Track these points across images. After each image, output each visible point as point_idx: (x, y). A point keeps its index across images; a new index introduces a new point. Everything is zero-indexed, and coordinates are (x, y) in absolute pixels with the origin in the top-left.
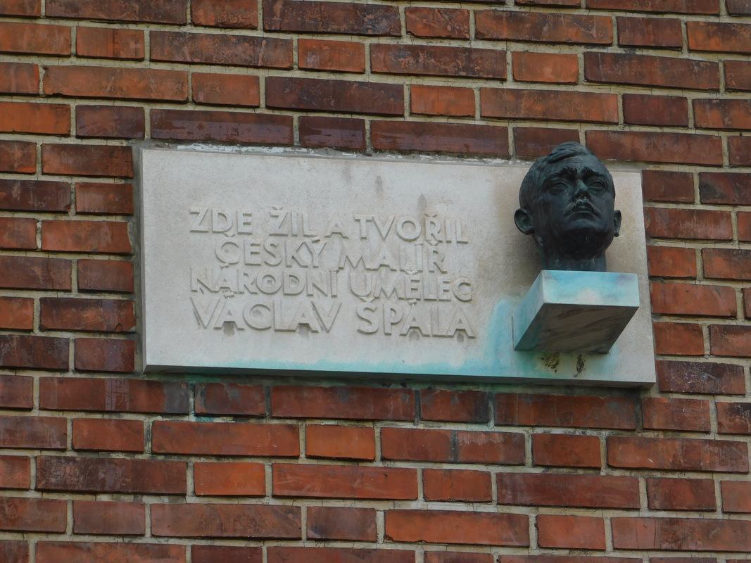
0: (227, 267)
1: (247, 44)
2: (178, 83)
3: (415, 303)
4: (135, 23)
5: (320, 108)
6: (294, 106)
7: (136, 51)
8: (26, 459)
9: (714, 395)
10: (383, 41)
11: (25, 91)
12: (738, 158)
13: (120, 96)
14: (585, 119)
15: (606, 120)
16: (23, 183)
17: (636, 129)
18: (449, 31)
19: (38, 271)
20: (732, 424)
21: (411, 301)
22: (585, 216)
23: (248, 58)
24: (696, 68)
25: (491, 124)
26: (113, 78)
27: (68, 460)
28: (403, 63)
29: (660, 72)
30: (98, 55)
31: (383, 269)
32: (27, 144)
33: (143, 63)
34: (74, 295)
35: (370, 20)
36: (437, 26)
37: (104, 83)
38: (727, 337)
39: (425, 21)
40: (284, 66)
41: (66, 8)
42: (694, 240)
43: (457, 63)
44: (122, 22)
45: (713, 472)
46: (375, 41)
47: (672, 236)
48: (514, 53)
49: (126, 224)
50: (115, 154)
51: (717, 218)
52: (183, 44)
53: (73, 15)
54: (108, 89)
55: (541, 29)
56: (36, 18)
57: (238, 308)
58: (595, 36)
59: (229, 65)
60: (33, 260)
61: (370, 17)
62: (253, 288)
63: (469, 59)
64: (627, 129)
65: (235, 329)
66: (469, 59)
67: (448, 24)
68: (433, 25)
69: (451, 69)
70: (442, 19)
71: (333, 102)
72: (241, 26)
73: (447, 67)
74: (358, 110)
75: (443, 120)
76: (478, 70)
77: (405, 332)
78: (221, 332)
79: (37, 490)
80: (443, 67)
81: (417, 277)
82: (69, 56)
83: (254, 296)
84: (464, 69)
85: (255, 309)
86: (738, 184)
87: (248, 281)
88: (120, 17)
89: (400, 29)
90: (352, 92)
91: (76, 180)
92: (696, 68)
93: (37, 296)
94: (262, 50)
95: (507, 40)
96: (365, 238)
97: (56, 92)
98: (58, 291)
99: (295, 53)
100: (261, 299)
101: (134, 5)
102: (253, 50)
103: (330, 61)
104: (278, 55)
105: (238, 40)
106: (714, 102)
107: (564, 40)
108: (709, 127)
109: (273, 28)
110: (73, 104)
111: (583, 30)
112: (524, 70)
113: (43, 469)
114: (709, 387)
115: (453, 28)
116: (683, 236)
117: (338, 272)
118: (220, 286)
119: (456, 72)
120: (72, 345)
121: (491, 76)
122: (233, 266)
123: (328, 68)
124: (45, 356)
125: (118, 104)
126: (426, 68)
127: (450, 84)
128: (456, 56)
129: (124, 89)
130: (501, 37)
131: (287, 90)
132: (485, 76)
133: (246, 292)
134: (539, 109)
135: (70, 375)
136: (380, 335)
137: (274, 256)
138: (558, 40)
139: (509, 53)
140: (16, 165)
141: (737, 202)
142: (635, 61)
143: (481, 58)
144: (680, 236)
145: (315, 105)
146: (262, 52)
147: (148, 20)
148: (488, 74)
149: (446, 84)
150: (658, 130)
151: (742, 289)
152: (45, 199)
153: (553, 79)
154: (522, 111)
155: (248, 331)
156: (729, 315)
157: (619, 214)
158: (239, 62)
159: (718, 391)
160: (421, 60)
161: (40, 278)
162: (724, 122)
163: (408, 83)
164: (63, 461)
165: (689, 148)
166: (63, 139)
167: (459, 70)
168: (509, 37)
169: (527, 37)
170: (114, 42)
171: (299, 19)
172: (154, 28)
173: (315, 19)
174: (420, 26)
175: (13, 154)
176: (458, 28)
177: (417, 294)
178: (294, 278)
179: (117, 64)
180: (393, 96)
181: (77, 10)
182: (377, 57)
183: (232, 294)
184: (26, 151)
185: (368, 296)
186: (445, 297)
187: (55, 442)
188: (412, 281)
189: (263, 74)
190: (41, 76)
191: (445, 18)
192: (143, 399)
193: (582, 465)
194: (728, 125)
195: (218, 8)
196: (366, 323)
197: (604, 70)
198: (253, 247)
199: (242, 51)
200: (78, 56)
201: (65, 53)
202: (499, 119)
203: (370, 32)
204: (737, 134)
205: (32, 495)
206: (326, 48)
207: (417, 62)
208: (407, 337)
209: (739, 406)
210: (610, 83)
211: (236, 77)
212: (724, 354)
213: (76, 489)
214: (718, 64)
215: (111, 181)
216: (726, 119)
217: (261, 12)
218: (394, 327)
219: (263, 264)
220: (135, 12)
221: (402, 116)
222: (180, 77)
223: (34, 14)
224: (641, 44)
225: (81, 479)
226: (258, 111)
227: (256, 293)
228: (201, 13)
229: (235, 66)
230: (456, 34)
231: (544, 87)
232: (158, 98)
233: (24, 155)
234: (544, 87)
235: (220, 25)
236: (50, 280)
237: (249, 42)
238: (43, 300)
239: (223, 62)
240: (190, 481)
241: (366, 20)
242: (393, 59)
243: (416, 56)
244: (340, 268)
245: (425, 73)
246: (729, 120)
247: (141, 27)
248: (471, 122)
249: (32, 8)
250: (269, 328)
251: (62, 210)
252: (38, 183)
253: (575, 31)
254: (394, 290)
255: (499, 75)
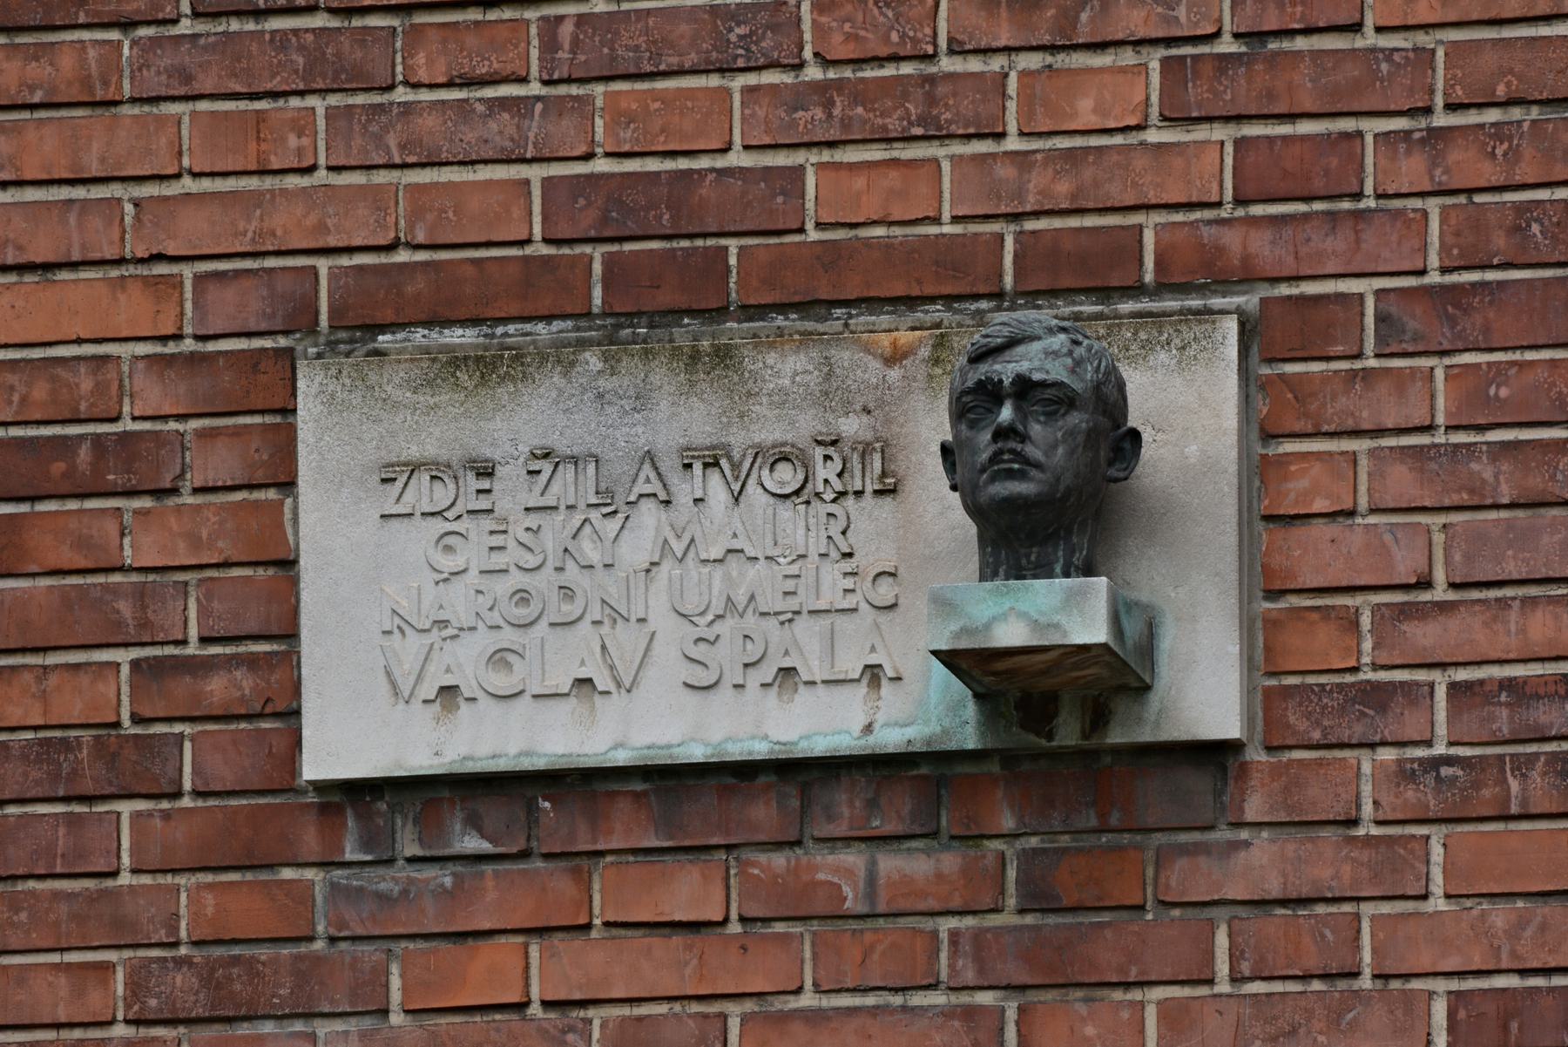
0: (446, 580)
1: (506, 116)
2: (379, 209)
3: (790, 621)
4: (301, 94)
5: (640, 233)
6: (593, 233)
7: (300, 151)
8: (108, 967)
9: (1372, 746)
10: (770, 78)
11: (97, 256)
12: (1455, 252)
13: (271, 248)
14: (1154, 201)
15: (1194, 199)
16: (97, 439)
17: (1258, 210)
18: (892, 44)
19: (125, 608)
20: (1399, 802)
21: (782, 618)
22: (1010, 475)
23: (508, 144)
24: (1384, 67)
25: (974, 228)
26: (258, 212)
27: (180, 962)
28: (802, 122)
29: (1309, 85)
30: (230, 168)
31: (733, 562)
32: (105, 358)
33: (316, 174)
34: (192, 649)
35: (741, 37)
36: (870, 36)
37: (241, 225)
38: (1404, 627)
39: (847, 26)
40: (576, 153)
41: (169, 77)
42: (1356, 433)
43: (907, 109)
44: (274, 95)
45: (1358, 899)
46: (752, 79)
47: (1310, 429)
48: (1024, 74)
49: (282, 503)
50: (262, 367)
51: (1401, 380)
52: (386, 129)
53: (182, 91)
54: (250, 234)
55: (1077, 17)
56: (115, 103)
57: (465, 661)
58: (1183, 19)
59: (473, 163)
60: (113, 590)
61: (740, 31)
62: (495, 618)
63: (931, 100)
64: (1240, 212)
65: (460, 700)
66: (931, 100)
67: (893, 28)
68: (862, 33)
69: (894, 125)
70: (882, 19)
71: (666, 217)
72: (497, 77)
73: (888, 120)
74: (713, 229)
75: (880, 231)
76: (946, 121)
77: (769, 680)
78: (437, 707)
79: (127, 1022)
80: (880, 121)
81: (794, 569)
82: (178, 176)
83: (494, 633)
84: (922, 121)
85: (498, 656)
86: (1450, 309)
87: (484, 602)
88: (269, 86)
89: (802, 49)
90: (704, 192)
91: (194, 424)
92: (1384, 67)
93: (123, 656)
94: (535, 124)
95: (1008, 50)
96: (701, 500)
97: (155, 252)
98: (162, 643)
99: (599, 122)
100: (509, 637)
101: (294, 57)
102: (518, 127)
103: (663, 131)
104: (566, 133)
105: (490, 108)
106: (1417, 135)
107: (1120, 36)
108: (1403, 191)
109: (556, 77)
110: (187, 271)
111: (1160, 10)
112: (1039, 110)
113: (136, 988)
114: (1358, 732)
115: (903, 36)
116: (1332, 428)
117: (648, 571)
118: (431, 619)
119: (904, 130)
120: (187, 745)
121: (972, 130)
122: (459, 577)
123: (661, 148)
124: (133, 767)
125: (271, 262)
126: (846, 124)
127: (895, 154)
128: (905, 96)
129: (279, 232)
130: (995, 44)
131: (582, 202)
132: (961, 132)
133: (480, 625)
134: (1063, 189)
135: (186, 802)
136: (726, 691)
137: (530, 549)
138: (1109, 38)
139: (1013, 76)
140: (83, 406)
141: (1446, 346)
142: (1259, 67)
143: (955, 95)
144: (1325, 428)
145: (632, 227)
146: (533, 128)
147: (321, 86)
148: (966, 126)
149: (886, 155)
150: (1301, 207)
151: (1444, 526)
152: (135, 470)
153: (1095, 122)
154: (1031, 198)
155: (484, 702)
156: (1413, 580)
157: (1135, 435)
158: (491, 154)
159: (1377, 738)
160: (837, 112)
161: (130, 621)
162: (1432, 178)
163: (814, 159)
164: (171, 965)
165: (1358, 241)
166: (171, 344)
167: (911, 124)
168: (1012, 43)
169: (1047, 39)
170: (258, 138)
171: (606, 50)
172: (334, 100)
173: (637, 48)
174: (837, 38)
175: (77, 385)
176: (911, 34)
177: (793, 603)
178: (567, 592)
179: (269, 182)
180: (784, 193)
181: (188, 79)
182: (753, 115)
183: (456, 632)
184: (100, 378)
185: (702, 614)
186: (847, 603)
187: (156, 931)
188: (786, 576)
189: (535, 173)
190: (128, 220)
191: (886, 16)
192: (310, 840)
193: (1107, 904)
194: (1440, 183)
195: (452, 46)
196: (699, 668)
197: (1196, 95)
198: (494, 537)
199: (500, 129)
200: (196, 175)
201: (170, 171)
202: (987, 218)
203: (741, 63)
204: (1462, 199)
205: (120, 1031)
206: (657, 105)
207: (830, 116)
208: (776, 688)
209: (1416, 766)
210: (1210, 119)
211: (489, 183)
212: (1399, 662)
213: (193, 1014)
214: (1433, 51)
215: (257, 419)
216: (1438, 172)
217: (535, 42)
218: (750, 671)
219: (513, 569)
220: (296, 71)
221: (801, 230)
222: (378, 198)
223: (110, 97)
224: (1274, 27)
225: (202, 996)
226: (529, 250)
227: (499, 627)
228: (421, 59)
229: (486, 162)
230: (908, 49)
231: (1078, 142)
232: (340, 244)
233: (97, 384)
234: (1078, 142)
235: (458, 81)
236: (144, 624)
237: (509, 111)
238: (135, 664)
239: (460, 157)
240: (395, 982)
241: (733, 37)
242: (783, 115)
243: (828, 105)
244: (652, 564)
245: (843, 137)
246: (1444, 173)
247: (312, 101)
248: (933, 230)
249: (106, 84)
250: (522, 692)
251: (168, 485)
252: (126, 435)
253: (1143, 14)
254: (752, 598)
255: (987, 126)
